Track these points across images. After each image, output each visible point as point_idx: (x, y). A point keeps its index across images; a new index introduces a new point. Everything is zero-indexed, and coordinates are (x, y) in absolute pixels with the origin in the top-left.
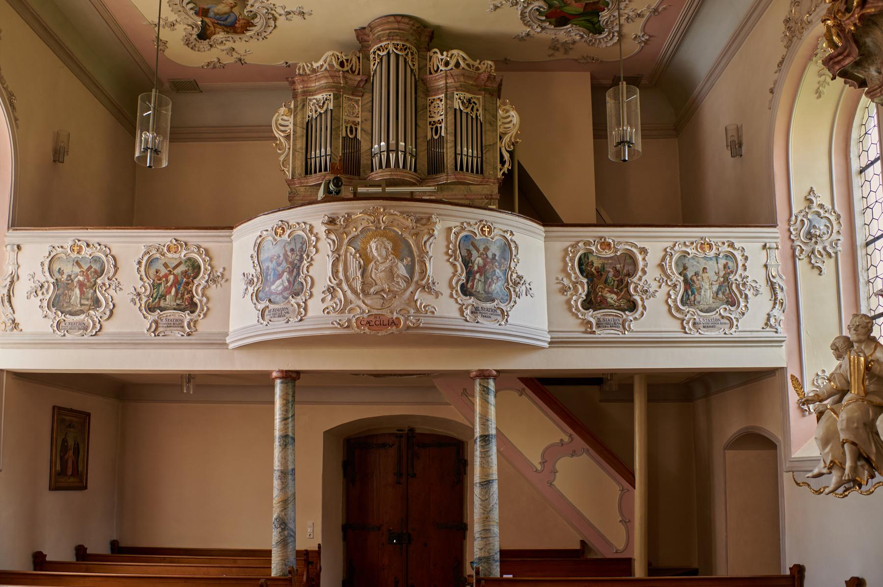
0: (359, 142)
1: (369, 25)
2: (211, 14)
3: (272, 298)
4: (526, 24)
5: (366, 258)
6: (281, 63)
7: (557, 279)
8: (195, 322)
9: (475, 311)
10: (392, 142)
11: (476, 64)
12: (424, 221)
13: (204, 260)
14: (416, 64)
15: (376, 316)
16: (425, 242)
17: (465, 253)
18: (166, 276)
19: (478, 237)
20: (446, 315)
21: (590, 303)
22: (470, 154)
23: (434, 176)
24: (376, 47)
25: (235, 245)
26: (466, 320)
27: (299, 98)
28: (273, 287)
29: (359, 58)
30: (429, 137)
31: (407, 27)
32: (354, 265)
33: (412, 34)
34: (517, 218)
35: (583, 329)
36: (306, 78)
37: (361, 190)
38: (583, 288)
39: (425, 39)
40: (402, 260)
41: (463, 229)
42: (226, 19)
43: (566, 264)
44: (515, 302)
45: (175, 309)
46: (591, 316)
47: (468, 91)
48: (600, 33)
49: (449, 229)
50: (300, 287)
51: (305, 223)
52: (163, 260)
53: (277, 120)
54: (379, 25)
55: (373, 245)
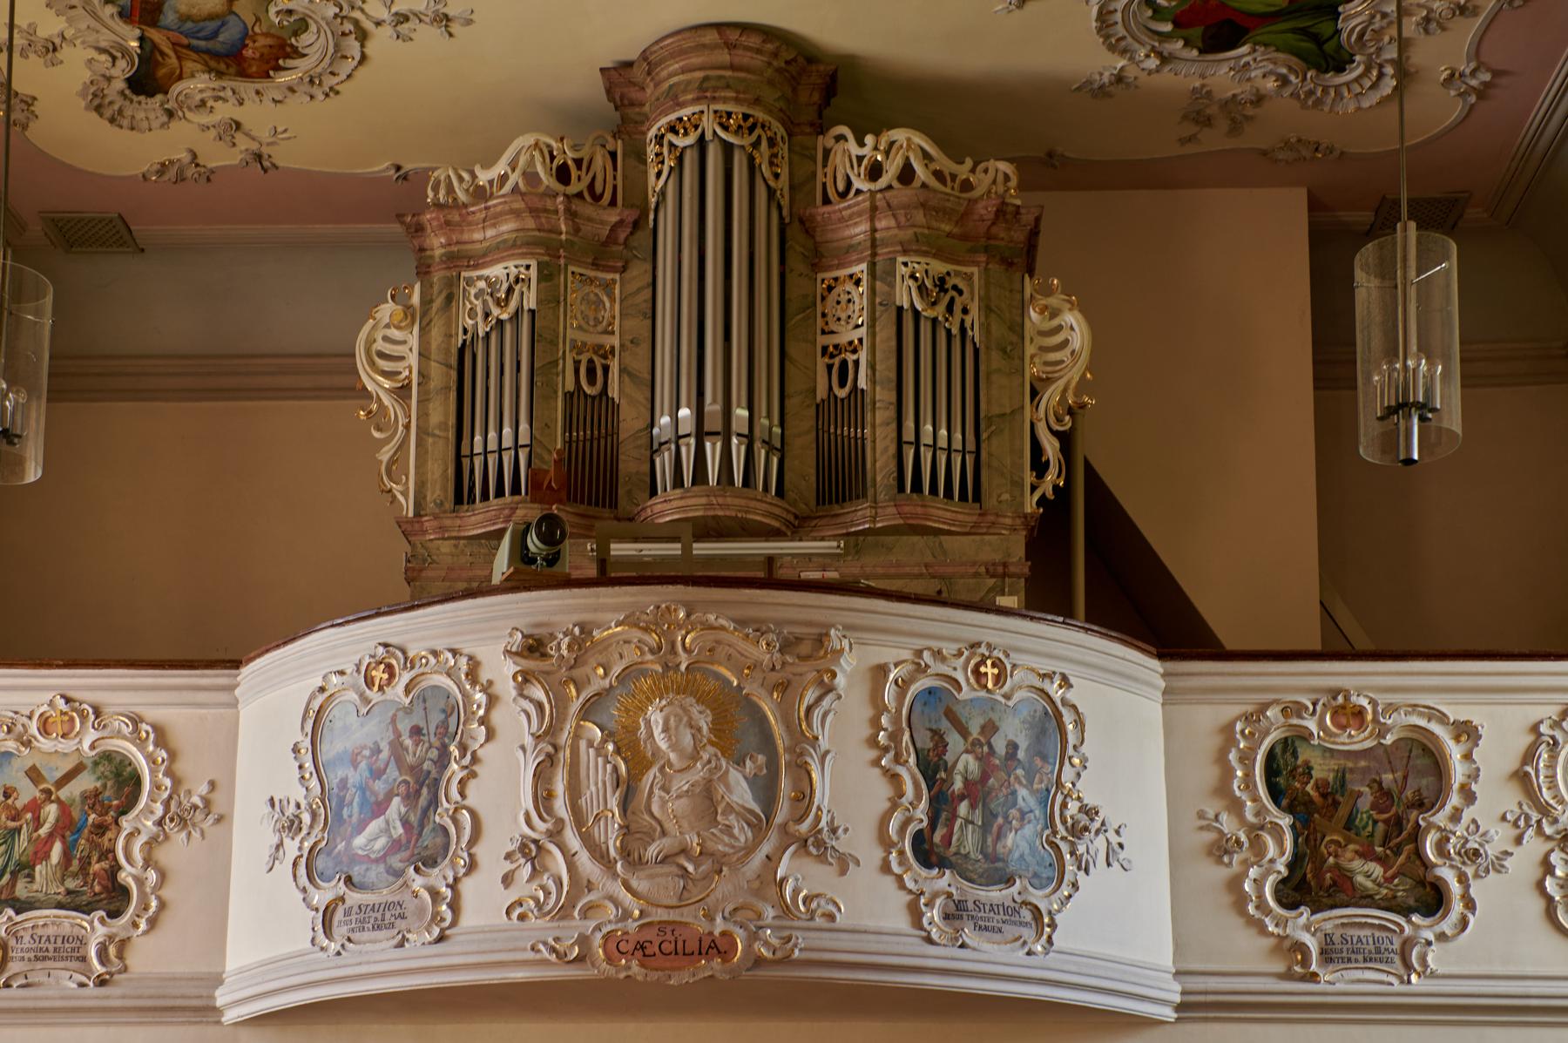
0: (613, 408)
1: (644, 56)
2: (169, 18)
3: (356, 872)
4: (1116, 47)
5: (634, 755)
6: (382, 166)
7: (1201, 815)
8: (123, 944)
9: (956, 913)
10: (712, 407)
11: (963, 170)
12: (805, 648)
13: (151, 759)
14: (784, 172)
15: (662, 926)
16: (809, 710)
17: (925, 741)
18: (35, 807)
19: (966, 694)
20: (871, 924)
21: (1298, 890)
22: (943, 443)
23: (837, 509)
24: (664, 121)
25: (249, 713)
26: (929, 940)
27: (437, 276)
28: (359, 841)
29: (613, 155)
30: (821, 393)
31: (758, 61)
32: (598, 775)
33: (770, 83)
34: (1081, 637)
35: (1280, 967)
36: (455, 217)
37: (618, 549)
38: (1280, 843)
39: (809, 96)
40: (740, 763)
41: (921, 670)
42: (215, 34)
43: (1228, 773)
44: (1075, 886)
45: (60, 906)
46: (1304, 926)
47: (939, 255)
48: (1340, 69)
49: (881, 671)
50: (439, 840)
51: (455, 652)
52: (26, 758)
53: (370, 342)
54: (672, 56)
55: (656, 717)
